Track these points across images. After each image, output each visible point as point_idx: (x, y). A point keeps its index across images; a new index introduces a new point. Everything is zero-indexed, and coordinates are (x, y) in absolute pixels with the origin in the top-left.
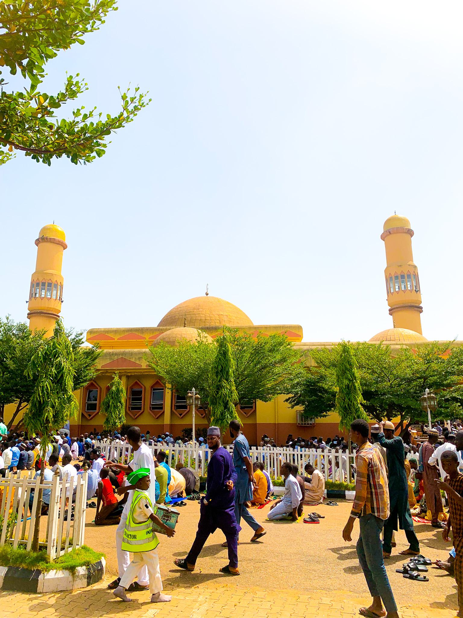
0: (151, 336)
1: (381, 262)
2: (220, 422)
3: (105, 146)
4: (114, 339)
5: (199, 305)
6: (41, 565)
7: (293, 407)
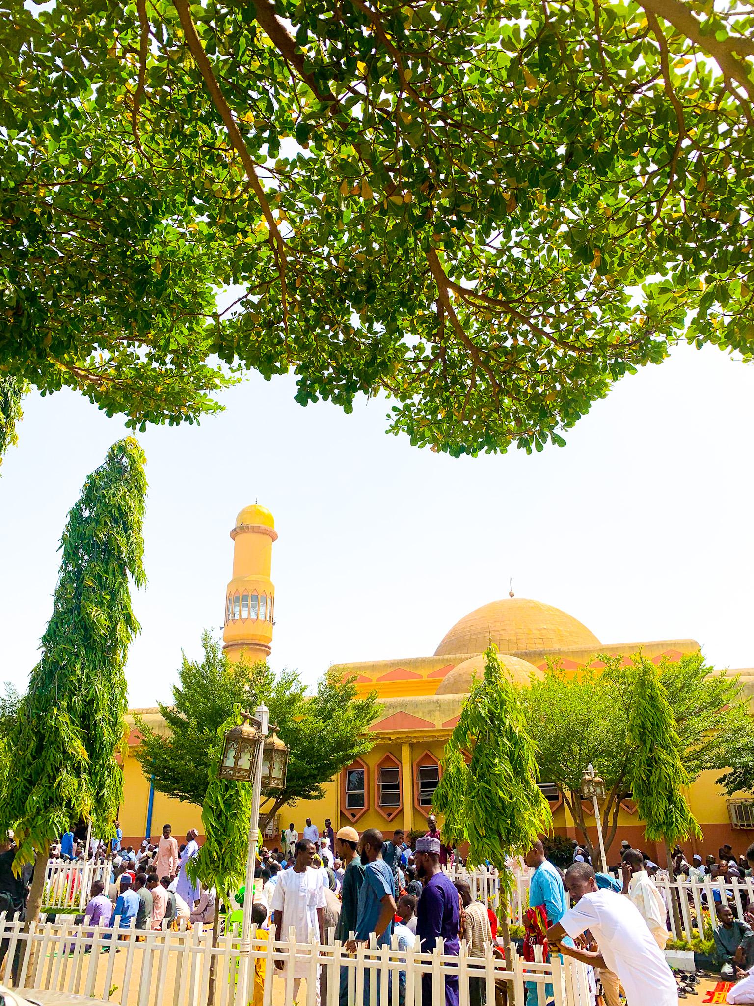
0: (431, 672)
2: (665, 828)
4: (371, 680)
7: (730, 793)
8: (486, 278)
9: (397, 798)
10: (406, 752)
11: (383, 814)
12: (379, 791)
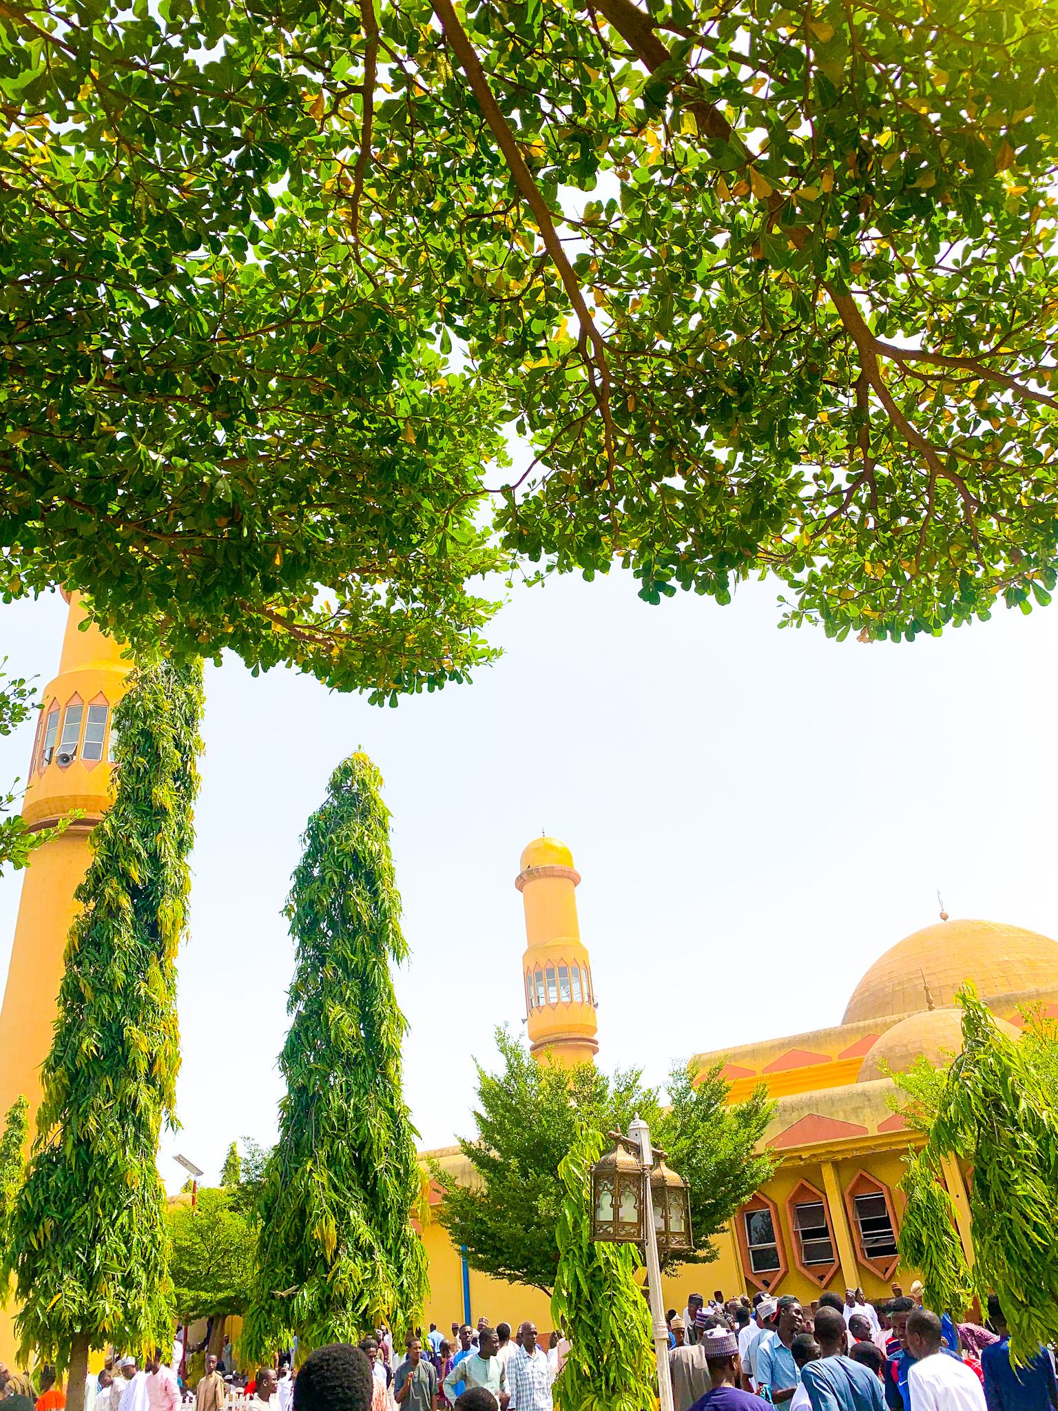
0: (842, 1049)
4: (753, 1073)
8: (936, 326)
9: (828, 1250)
10: (828, 1174)
11: (812, 1278)
12: (798, 1241)
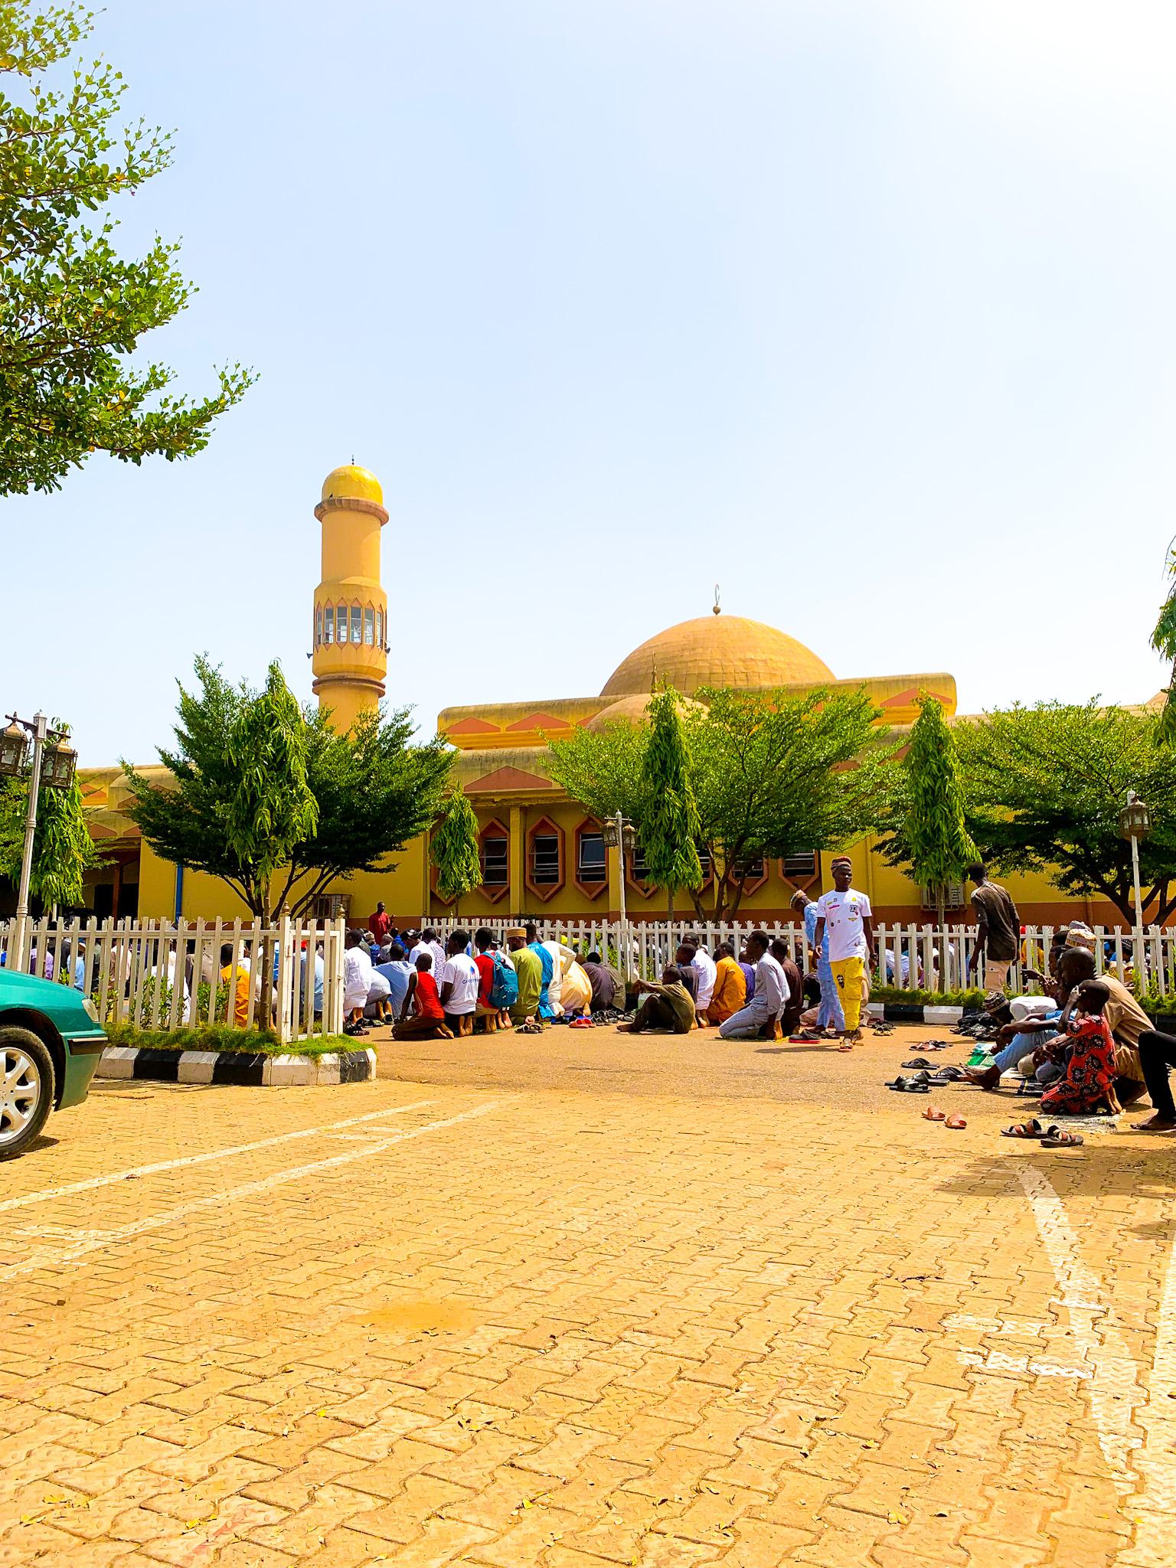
1: (307, 574)
3: (207, 435)
5: (695, 640)
6: (267, 1048)
9: (503, 875)
10: (515, 818)
